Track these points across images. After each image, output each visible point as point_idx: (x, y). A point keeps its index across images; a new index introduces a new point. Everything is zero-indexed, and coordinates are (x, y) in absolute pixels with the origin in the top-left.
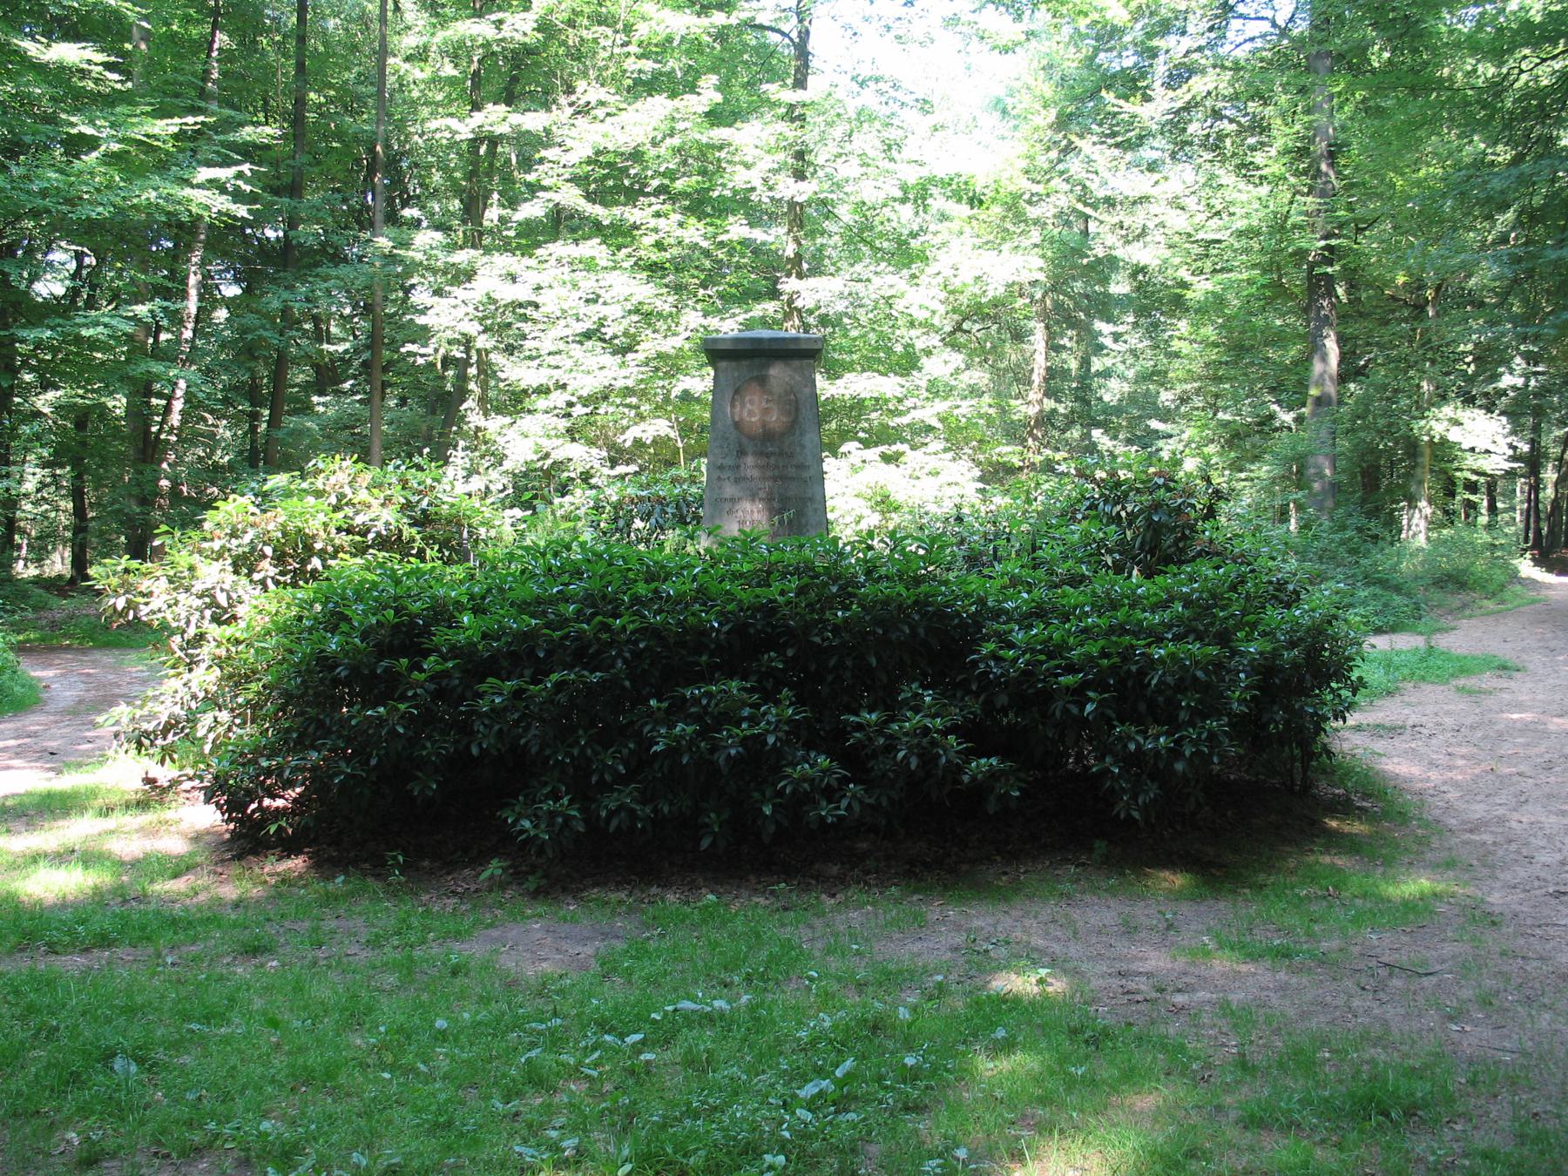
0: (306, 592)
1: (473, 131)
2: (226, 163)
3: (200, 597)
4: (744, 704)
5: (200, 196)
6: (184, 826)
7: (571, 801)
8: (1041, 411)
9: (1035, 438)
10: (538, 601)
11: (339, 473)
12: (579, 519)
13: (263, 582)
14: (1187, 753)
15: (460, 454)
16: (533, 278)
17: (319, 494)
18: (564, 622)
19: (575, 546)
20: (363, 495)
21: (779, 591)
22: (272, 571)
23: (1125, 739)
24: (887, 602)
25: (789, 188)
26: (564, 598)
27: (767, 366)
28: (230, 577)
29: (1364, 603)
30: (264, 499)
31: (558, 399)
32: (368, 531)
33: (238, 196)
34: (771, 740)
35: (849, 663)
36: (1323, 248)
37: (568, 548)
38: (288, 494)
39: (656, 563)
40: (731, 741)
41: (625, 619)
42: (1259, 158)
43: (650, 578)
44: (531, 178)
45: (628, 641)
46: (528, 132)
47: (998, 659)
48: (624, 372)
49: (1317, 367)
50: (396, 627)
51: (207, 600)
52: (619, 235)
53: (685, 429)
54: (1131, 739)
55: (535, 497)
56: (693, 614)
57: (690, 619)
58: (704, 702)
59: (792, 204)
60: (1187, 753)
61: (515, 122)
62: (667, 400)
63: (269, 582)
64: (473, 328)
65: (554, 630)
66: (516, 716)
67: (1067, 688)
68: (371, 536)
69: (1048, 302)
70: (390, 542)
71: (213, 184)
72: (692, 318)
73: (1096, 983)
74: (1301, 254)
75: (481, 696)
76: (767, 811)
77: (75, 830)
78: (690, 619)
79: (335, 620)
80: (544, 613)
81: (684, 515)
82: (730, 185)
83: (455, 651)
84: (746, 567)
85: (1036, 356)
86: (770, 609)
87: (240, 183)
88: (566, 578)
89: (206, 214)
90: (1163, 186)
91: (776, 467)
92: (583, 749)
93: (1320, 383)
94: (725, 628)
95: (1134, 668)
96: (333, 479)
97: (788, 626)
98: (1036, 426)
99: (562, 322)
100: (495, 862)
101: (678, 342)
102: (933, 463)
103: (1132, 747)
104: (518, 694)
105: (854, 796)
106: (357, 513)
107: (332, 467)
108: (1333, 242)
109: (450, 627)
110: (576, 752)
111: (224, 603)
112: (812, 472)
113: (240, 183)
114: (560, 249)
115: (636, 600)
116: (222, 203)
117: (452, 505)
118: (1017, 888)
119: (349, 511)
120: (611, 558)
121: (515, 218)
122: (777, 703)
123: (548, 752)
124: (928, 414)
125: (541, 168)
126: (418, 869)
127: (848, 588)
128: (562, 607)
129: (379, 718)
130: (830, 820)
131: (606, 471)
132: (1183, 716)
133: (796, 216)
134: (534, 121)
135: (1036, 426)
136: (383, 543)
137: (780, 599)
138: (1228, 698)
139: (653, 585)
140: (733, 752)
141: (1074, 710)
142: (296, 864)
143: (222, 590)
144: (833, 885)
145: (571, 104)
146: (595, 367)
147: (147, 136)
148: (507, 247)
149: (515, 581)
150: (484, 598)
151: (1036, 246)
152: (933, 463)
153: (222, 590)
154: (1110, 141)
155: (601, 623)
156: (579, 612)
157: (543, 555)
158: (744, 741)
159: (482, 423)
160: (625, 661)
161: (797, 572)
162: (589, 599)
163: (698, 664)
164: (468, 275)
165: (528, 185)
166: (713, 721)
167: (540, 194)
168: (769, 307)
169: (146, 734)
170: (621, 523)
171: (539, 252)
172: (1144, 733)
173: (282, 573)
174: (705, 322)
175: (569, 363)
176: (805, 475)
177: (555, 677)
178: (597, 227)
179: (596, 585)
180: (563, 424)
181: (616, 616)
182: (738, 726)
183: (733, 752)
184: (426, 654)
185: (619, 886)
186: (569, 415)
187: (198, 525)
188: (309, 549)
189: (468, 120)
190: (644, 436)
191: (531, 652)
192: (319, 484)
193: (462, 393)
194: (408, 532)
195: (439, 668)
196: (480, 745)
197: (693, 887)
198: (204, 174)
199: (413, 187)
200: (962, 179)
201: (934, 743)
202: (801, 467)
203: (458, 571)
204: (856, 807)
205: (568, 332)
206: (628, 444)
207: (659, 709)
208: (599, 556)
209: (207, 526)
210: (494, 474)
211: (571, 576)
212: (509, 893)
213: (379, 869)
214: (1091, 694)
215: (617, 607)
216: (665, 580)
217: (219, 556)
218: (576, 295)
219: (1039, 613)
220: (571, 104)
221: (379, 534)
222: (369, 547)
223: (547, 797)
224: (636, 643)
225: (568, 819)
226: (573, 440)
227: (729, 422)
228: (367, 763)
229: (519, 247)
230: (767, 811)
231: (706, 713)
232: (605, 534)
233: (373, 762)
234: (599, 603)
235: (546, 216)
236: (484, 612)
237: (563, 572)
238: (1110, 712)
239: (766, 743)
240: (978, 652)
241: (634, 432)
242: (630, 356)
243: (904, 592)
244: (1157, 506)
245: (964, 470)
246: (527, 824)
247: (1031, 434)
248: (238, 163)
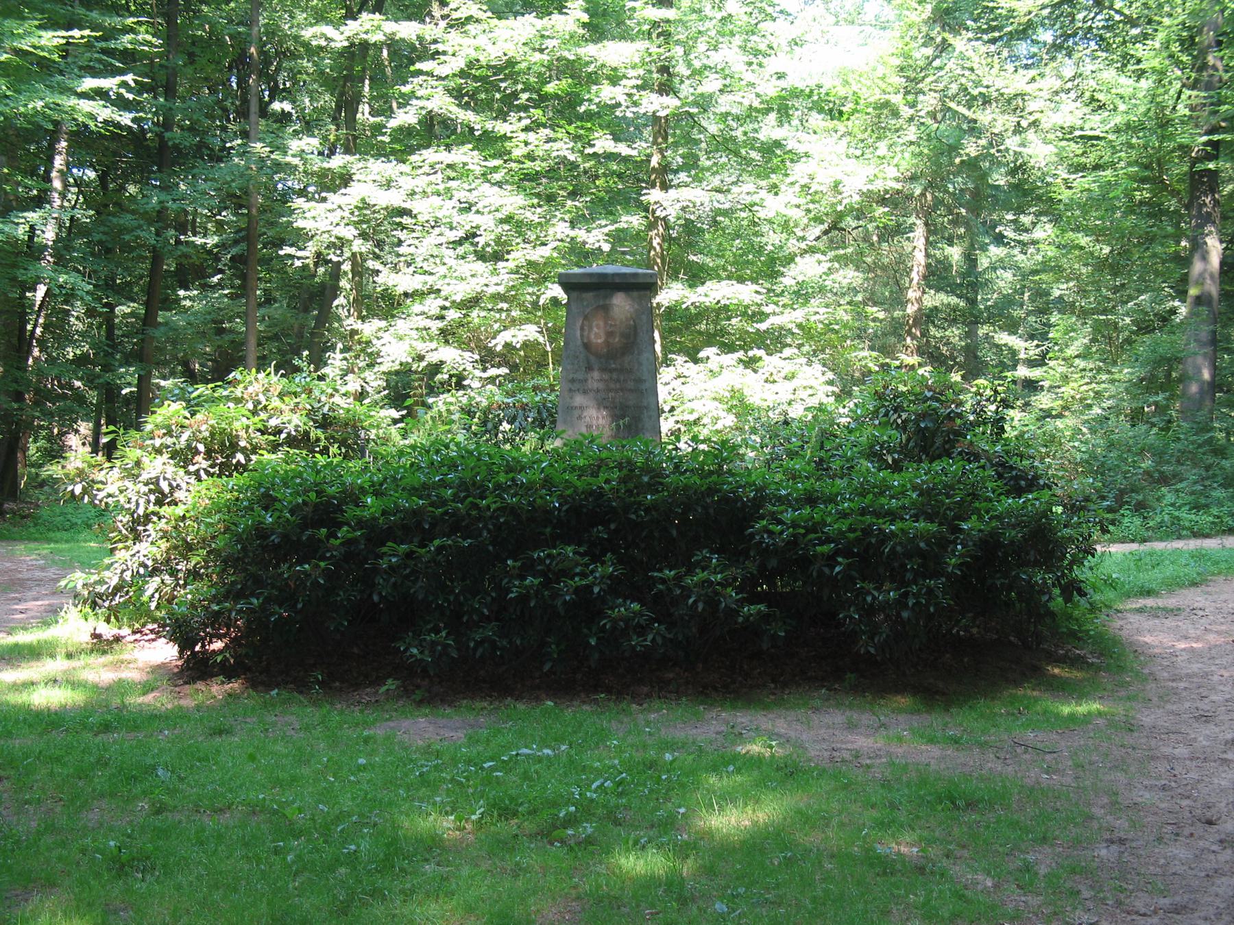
0: (237, 480)
1: (348, 39)
2: (114, 72)
3: (146, 484)
4: (577, 564)
5: (86, 106)
6: (140, 665)
7: (448, 634)
8: (920, 309)
9: (914, 337)
10: (425, 486)
11: (255, 384)
12: (453, 421)
13: (197, 473)
14: (910, 604)
15: (339, 356)
16: (407, 183)
17: (238, 401)
18: (443, 502)
19: (452, 446)
20: (276, 403)
21: (608, 480)
22: (205, 464)
23: (862, 593)
24: (686, 488)
25: (653, 103)
26: (444, 484)
27: (611, 296)
28: (170, 470)
29: (1220, 504)
30: (193, 407)
31: (432, 305)
32: (280, 432)
33: (122, 104)
34: (596, 590)
35: (656, 534)
36: (1205, 144)
37: (447, 447)
38: (213, 401)
39: (513, 458)
40: (567, 589)
41: (490, 500)
42: (1138, 50)
43: (509, 469)
44: (406, 89)
45: (491, 517)
46: (403, 40)
47: (771, 533)
48: (495, 279)
49: (1197, 267)
50: (316, 505)
51: (152, 487)
52: (488, 142)
53: (552, 334)
54: (869, 593)
55: (416, 403)
56: (541, 497)
57: (539, 501)
58: (548, 562)
59: (655, 118)
60: (910, 604)
61: (388, 31)
62: (535, 304)
63: (202, 472)
64: (349, 233)
65: (437, 508)
66: (408, 571)
67: (823, 554)
68: (283, 436)
69: (929, 197)
70: (300, 441)
71: (101, 94)
72: (560, 229)
73: (813, 753)
74: (1185, 149)
75: (381, 556)
76: (593, 642)
77: (55, 666)
78: (539, 501)
79: (268, 501)
80: (429, 496)
81: (545, 419)
82: (597, 100)
83: (361, 523)
84: (581, 462)
85: (916, 253)
86: (599, 494)
87: (123, 91)
88: (445, 469)
89: (92, 124)
90: (1041, 83)
91: (618, 380)
92: (457, 595)
93: (1200, 282)
94: (565, 508)
95: (873, 541)
96: (250, 389)
97: (613, 507)
98: (915, 324)
99: (437, 231)
100: (390, 681)
101: (546, 252)
102: (788, 367)
103: (869, 599)
104: (409, 555)
105: (658, 633)
106: (270, 417)
107: (248, 379)
108: (1216, 137)
109: (357, 506)
110: (452, 598)
111: (166, 489)
112: (647, 385)
113: (123, 91)
114: (431, 155)
115: (498, 486)
116: (105, 112)
117: (348, 411)
118: (780, 703)
119: (263, 416)
120: (480, 454)
121: (389, 125)
122: (603, 563)
123: (431, 598)
124: (788, 318)
125: (415, 80)
126: (331, 688)
127: (656, 474)
128: (442, 491)
129: (305, 572)
130: (638, 648)
131: (478, 373)
132: (909, 576)
133: (660, 126)
134: (408, 30)
135: (915, 324)
136: (292, 441)
137: (606, 487)
138: (946, 563)
139: (511, 475)
140: (568, 598)
141: (827, 570)
142: (235, 685)
143: (165, 479)
144: (637, 698)
145: (443, 17)
146: (468, 274)
147: (34, 47)
148: (382, 153)
149: (406, 471)
150: (381, 485)
151: (912, 143)
152: (788, 367)
153: (165, 479)
154: (985, 37)
155: (471, 503)
156: (455, 495)
157: (428, 452)
158: (577, 590)
159: (358, 325)
160: (489, 531)
161: (620, 466)
162: (463, 485)
163: (544, 534)
164: (345, 179)
165: (402, 95)
166: (552, 576)
167: (414, 102)
168: (633, 221)
169: (100, 596)
170: (490, 425)
171: (413, 158)
172: (878, 589)
173: (212, 466)
174: (572, 233)
175: (442, 270)
176: (643, 387)
177: (437, 542)
178: (468, 135)
179: (468, 475)
180: (436, 326)
181: (483, 498)
182: (572, 579)
183: (568, 598)
184: (340, 525)
185: (483, 698)
186: (442, 318)
187: (138, 428)
188: (234, 447)
189: (342, 28)
190: (514, 340)
191: (419, 524)
192: (238, 392)
193: (335, 291)
194: (316, 433)
195: (350, 536)
196: (380, 594)
197: (538, 699)
198: (89, 83)
199: (283, 80)
200: (823, 91)
201: (716, 593)
202: (640, 381)
203: (355, 465)
204: (659, 640)
205: (442, 240)
206: (499, 348)
207: (514, 567)
208: (470, 453)
209: (149, 427)
210: (368, 375)
211: (450, 469)
212: (401, 703)
213: (302, 686)
214: (840, 559)
215: (484, 491)
216: (520, 472)
217: (159, 451)
218: (450, 204)
219: (811, 499)
220: (443, 17)
221: (289, 434)
222: (281, 445)
223: (430, 631)
224: (497, 518)
225: (446, 646)
226: (447, 342)
227: (579, 342)
228: (295, 606)
229: (394, 152)
230: (593, 642)
231: (549, 570)
232: (475, 435)
233: (300, 606)
234: (468, 488)
235: (420, 122)
236: (382, 494)
237: (442, 464)
238: (854, 573)
239: (592, 592)
240: (753, 527)
241: (505, 337)
242: (501, 264)
243: (698, 482)
244: (923, 416)
245: (819, 374)
246: (415, 651)
247: (909, 333)
248: (122, 72)
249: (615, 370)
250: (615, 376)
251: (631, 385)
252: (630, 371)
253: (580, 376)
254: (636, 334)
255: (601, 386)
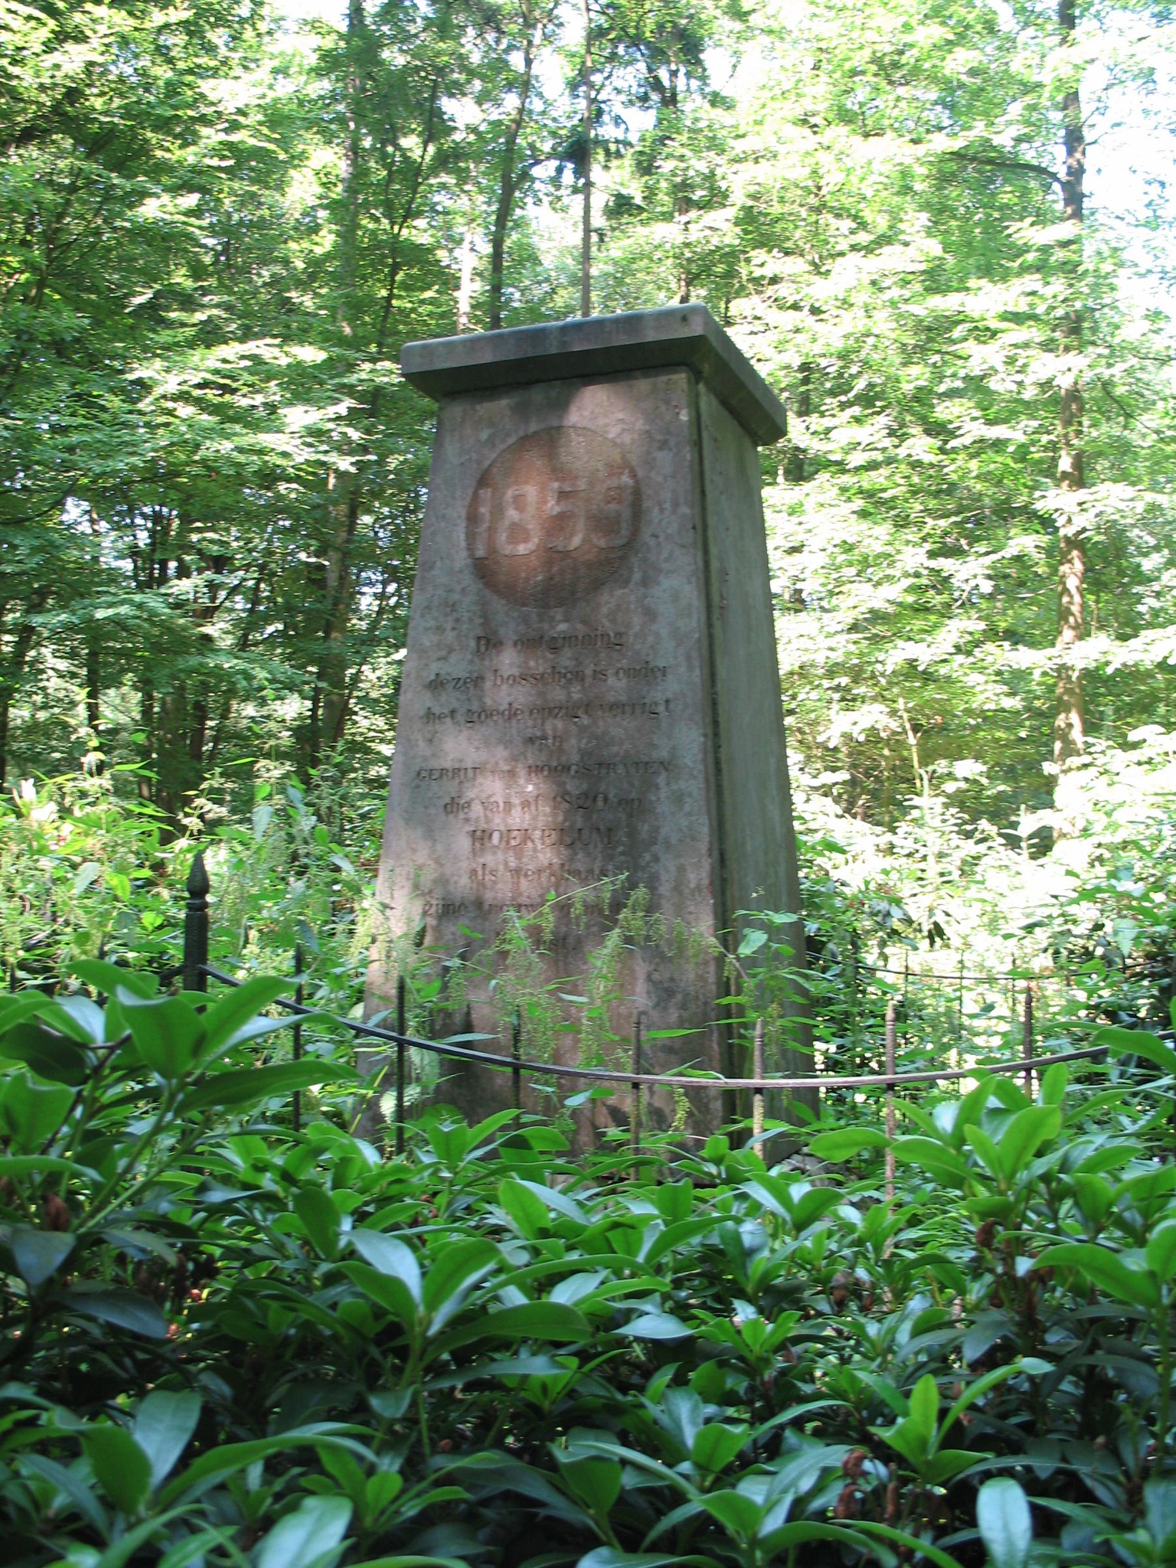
227: (461, 559)
249: (568, 639)
250: (566, 659)
251: (616, 686)
252: (616, 644)
253: (457, 666)
254: (637, 512)
255: (522, 696)
